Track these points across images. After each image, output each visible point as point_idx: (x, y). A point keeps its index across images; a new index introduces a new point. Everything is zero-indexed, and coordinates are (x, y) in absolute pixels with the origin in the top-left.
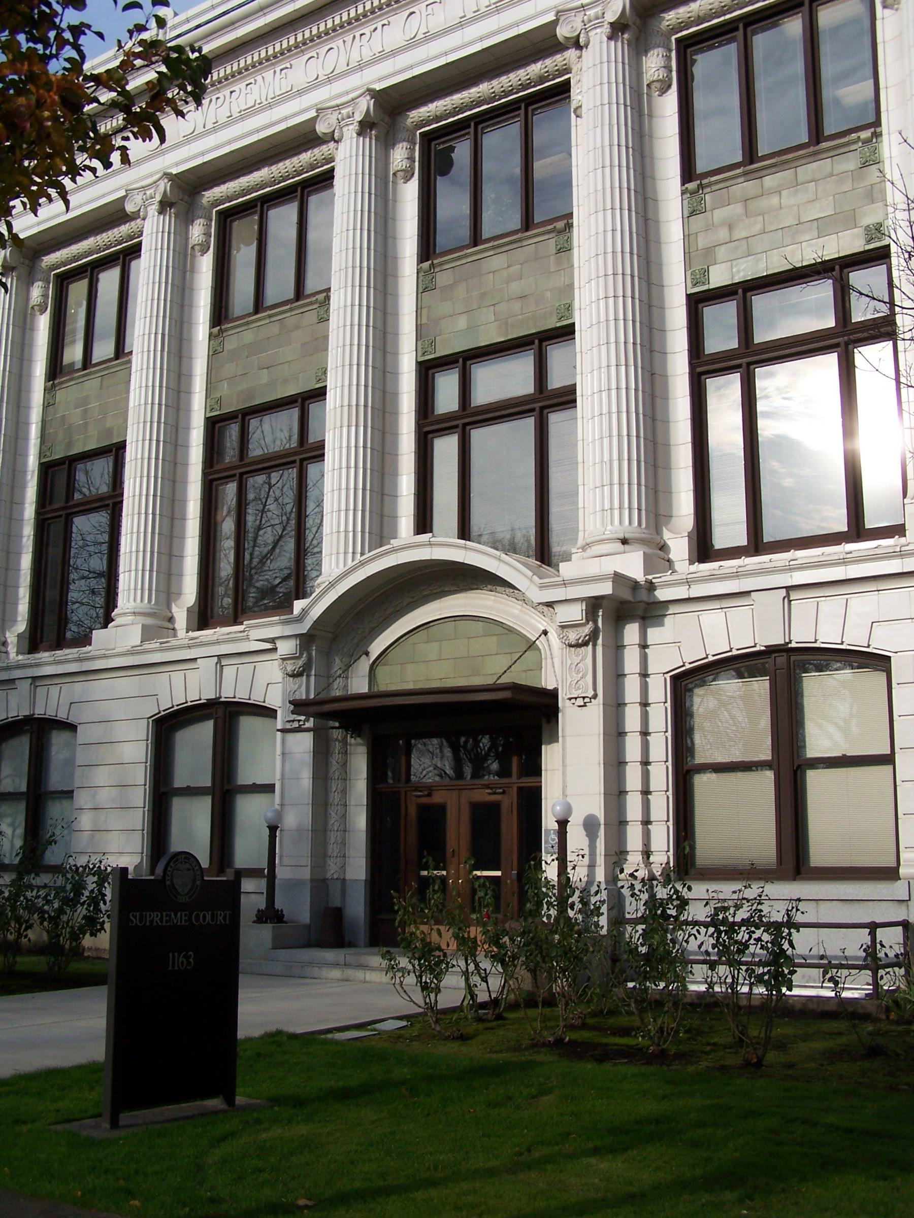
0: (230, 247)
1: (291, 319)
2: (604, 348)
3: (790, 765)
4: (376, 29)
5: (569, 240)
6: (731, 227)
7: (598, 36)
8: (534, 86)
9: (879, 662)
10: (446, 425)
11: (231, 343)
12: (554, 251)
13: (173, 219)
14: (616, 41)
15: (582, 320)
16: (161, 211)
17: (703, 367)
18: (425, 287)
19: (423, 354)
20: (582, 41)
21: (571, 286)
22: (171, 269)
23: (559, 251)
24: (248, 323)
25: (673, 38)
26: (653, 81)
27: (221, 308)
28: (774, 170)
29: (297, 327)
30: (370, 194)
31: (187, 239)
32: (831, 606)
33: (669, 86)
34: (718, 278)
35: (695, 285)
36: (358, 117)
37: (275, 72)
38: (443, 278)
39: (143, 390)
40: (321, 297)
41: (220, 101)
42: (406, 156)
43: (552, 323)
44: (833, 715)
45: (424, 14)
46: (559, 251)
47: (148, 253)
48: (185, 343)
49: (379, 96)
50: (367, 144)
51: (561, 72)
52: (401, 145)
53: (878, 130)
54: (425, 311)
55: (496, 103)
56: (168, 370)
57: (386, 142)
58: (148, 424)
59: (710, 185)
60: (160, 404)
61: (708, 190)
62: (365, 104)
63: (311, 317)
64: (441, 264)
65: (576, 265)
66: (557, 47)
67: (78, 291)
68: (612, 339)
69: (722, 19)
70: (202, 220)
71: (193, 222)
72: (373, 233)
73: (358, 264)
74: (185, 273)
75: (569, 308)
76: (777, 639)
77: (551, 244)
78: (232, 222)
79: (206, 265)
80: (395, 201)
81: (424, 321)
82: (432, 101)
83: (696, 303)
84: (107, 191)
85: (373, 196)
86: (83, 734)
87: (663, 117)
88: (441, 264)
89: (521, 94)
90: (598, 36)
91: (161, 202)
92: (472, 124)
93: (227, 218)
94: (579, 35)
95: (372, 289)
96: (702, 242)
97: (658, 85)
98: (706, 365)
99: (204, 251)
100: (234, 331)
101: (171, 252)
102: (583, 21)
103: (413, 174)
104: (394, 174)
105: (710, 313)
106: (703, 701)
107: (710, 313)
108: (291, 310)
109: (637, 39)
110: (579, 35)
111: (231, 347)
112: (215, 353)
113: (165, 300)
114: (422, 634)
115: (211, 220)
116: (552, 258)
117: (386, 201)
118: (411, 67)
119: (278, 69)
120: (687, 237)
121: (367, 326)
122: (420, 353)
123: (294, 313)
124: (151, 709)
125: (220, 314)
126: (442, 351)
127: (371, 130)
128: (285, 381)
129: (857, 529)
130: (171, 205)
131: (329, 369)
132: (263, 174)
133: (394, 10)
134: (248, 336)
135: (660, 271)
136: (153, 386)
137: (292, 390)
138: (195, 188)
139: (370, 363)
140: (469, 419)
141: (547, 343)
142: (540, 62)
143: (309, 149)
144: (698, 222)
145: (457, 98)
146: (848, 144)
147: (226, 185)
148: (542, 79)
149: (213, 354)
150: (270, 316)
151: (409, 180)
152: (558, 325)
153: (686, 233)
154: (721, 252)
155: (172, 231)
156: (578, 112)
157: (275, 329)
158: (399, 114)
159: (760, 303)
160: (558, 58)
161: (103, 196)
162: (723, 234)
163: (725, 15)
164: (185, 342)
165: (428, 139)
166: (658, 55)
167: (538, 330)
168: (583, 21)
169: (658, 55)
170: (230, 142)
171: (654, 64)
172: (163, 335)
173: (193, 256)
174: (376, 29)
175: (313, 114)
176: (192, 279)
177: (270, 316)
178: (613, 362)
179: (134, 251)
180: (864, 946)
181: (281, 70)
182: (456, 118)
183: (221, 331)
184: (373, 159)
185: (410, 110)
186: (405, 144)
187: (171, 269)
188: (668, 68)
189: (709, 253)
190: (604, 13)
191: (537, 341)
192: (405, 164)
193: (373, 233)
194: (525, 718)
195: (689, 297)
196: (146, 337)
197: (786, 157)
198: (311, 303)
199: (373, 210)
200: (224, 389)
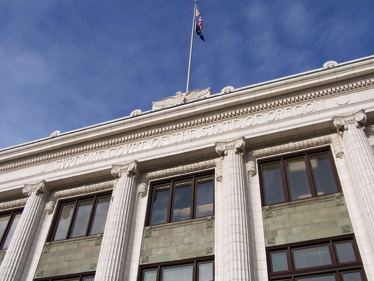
0: (60, 215)
1: (83, 243)
2: (235, 262)
4: (141, 143)
5: (213, 223)
6: (283, 223)
7: (232, 152)
8: (200, 170)
11: (54, 249)
12: (206, 227)
13: (41, 198)
14: (238, 155)
16: (37, 194)
18: (146, 236)
19: (142, 262)
20: (225, 153)
21: (213, 242)
22: (35, 216)
23: (208, 227)
24: (63, 242)
25: (256, 159)
26: (250, 171)
27: (51, 236)
28: (300, 204)
29: (85, 246)
30: (129, 197)
31: (44, 207)
33: (256, 174)
34: (280, 241)
35: (269, 244)
36: (129, 169)
37: (97, 153)
38: (154, 234)
39: (10, 261)
40: (99, 236)
41: (72, 160)
42: (144, 188)
43: (204, 254)
45: (161, 140)
46: (208, 227)
47: (27, 208)
48: (33, 246)
49: (140, 165)
50: (131, 180)
51: (211, 166)
52: (143, 184)
53: (342, 194)
54: (145, 245)
55: (184, 174)
56: (23, 255)
57: (138, 182)
58: (7, 276)
59: (274, 208)
60: (15, 269)
61: (273, 209)
62: (133, 165)
63: (93, 243)
64: (154, 228)
65: (216, 232)
68: (239, 258)
69: (276, 155)
70: (52, 202)
71: (48, 201)
72: (128, 211)
73: (121, 221)
74: (40, 219)
75: (212, 249)
77: (205, 225)
78: (63, 205)
79: (49, 219)
80: (138, 203)
81: (144, 249)
82: (158, 170)
83: (270, 250)
84: (17, 184)
85: (130, 198)
87: (253, 184)
88: (154, 228)
89: (194, 172)
90: (232, 152)
91: (38, 191)
92: (172, 181)
93: (62, 203)
94: (224, 151)
95: (125, 232)
96: (272, 228)
97: (252, 172)
98: (275, 276)
99: (50, 213)
100: (55, 245)
101: (37, 210)
102: (226, 147)
103: (146, 195)
104: (139, 193)
108: (84, 239)
109: (245, 155)
110: (224, 151)
111: (51, 251)
112: (45, 252)
113: (30, 227)
115: (56, 203)
116: (205, 230)
117: (134, 202)
118: (154, 156)
119: (98, 152)
120: (265, 226)
121: (121, 246)
122: (141, 262)
123: (84, 241)
125: (51, 237)
126: (151, 261)
127: (133, 176)
130: (42, 193)
131: (98, 264)
133: (149, 138)
134: (62, 247)
135: (254, 237)
136: (15, 260)
137: (77, 271)
138: (52, 190)
139: (120, 261)
141: (200, 263)
142: (204, 161)
143: (104, 182)
144: (269, 221)
146: (330, 197)
147: (66, 190)
148: (204, 167)
149: (44, 253)
150: (74, 241)
151: (144, 197)
152: (206, 255)
153: (265, 224)
154: (279, 233)
155: (40, 202)
156: (219, 179)
157: (75, 246)
158: (144, 173)
161: (14, 186)
162: (281, 226)
163: (276, 154)
164: (33, 246)
165: (153, 184)
166: (252, 163)
167: (197, 256)
168: (226, 147)
169: (252, 163)
170: (73, 173)
171: (251, 165)
172: (25, 240)
173: (45, 214)
174: (141, 143)
175: (111, 167)
176: (42, 223)
177: (74, 241)
178: (240, 268)
179: (20, 211)
181: (100, 152)
182: (166, 178)
183: (50, 244)
184: (132, 186)
185: (148, 172)
186: (145, 184)
187: (35, 216)
188: (255, 167)
189: (275, 233)
190: (234, 145)
191: (195, 262)
192: (144, 190)
193: (128, 211)
195: (267, 248)
196: (18, 240)
198: (94, 237)
199: (129, 203)
200: (45, 268)
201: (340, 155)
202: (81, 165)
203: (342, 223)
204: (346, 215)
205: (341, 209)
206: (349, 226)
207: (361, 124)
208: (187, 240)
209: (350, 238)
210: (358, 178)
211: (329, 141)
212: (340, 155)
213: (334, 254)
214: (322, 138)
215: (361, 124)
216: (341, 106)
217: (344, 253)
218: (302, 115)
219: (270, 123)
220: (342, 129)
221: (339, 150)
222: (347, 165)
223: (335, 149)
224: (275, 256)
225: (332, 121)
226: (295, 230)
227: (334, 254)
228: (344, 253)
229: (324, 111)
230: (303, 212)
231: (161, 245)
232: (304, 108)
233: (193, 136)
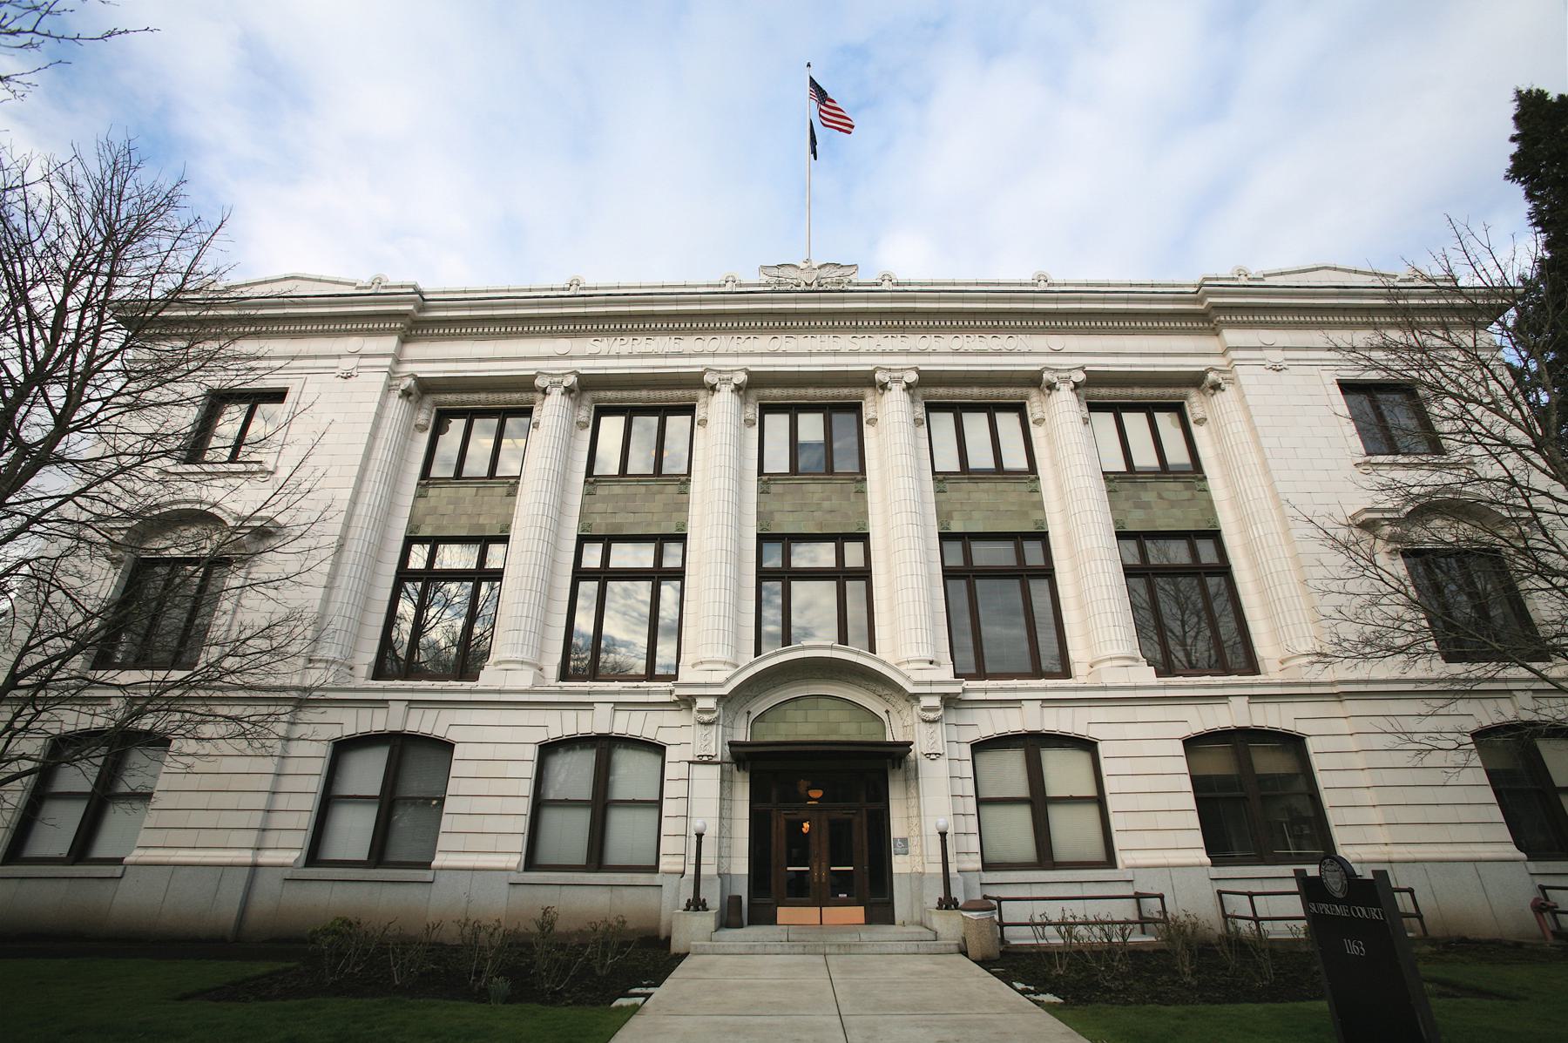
3: (601, 804)
5: (516, 490)
9: (659, 749)
10: (589, 575)
15: (515, 535)
17: (580, 574)
21: (866, 513)
32: (431, 714)
34: (956, 527)
44: (630, 775)
66: (533, 389)
67: (457, 426)
75: (508, 526)
76: (605, 730)
86: (458, 752)
96: (946, 508)
105: (416, 548)
106: (1081, 759)
107: (416, 548)
114: (793, 704)
124: (542, 736)
128: (649, 524)
129: (650, 675)
132: (644, 394)
140: (605, 575)
145: (625, 394)
154: (955, 515)
159: (616, 548)
160: (530, 395)
180: (1152, 906)
189: (949, 515)
194: (890, 760)
197: (812, 476)
201: (873, 421)
202: (643, 356)
203: (1037, 516)
204: (1040, 506)
205: (1035, 497)
206: (1044, 522)
207: (568, 391)
208: (826, 504)
209: (1042, 537)
210: (1253, 458)
211: (1185, 397)
212: (873, 421)
213: (1020, 554)
214: (853, 391)
215: (568, 391)
216: (1057, 352)
217: (1207, 553)
218: (998, 353)
219: (956, 353)
220: (1051, 387)
221: (1037, 416)
222: (1049, 437)
223: (868, 411)
224: (767, 547)
225: (703, 373)
226: (976, 515)
227: (1020, 554)
228: (1207, 553)
229: (1030, 353)
230: (987, 491)
231: (787, 507)
232: (1003, 342)
233: (649, 349)
